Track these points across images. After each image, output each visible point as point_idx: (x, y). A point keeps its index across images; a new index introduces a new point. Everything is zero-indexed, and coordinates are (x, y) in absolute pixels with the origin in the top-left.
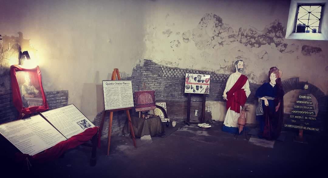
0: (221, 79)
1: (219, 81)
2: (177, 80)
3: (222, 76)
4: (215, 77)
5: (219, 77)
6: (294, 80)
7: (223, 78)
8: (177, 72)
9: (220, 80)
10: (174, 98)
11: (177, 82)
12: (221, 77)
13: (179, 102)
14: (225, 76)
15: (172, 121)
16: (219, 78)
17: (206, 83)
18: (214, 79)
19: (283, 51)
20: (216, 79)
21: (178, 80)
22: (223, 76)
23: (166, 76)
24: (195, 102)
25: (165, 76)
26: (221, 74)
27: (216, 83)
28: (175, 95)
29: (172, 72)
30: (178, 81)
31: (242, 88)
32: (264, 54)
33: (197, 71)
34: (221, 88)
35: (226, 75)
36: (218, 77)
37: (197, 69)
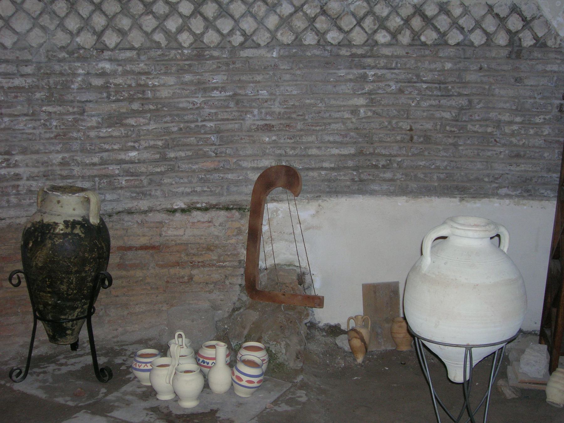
1: (344, 52)
2: (20, 62)
3: (362, 13)
4: (314, 19)
5: (339, 17)
9: (349, 44)
10: (13, 200)
11: (18, 82)
12: (359, 22)
13: (204, 83)
15: (464, 36)
16: (340, 29)
17: (189, 125)
18: (310, 39)
20: (321, 34)
21: (27, 63)
24: (185, 217)
27: (327, 64)
28: (18, 177)
30: (29, 70)
31: (99, 369)
32: (178, 215)
34: (362, 101)
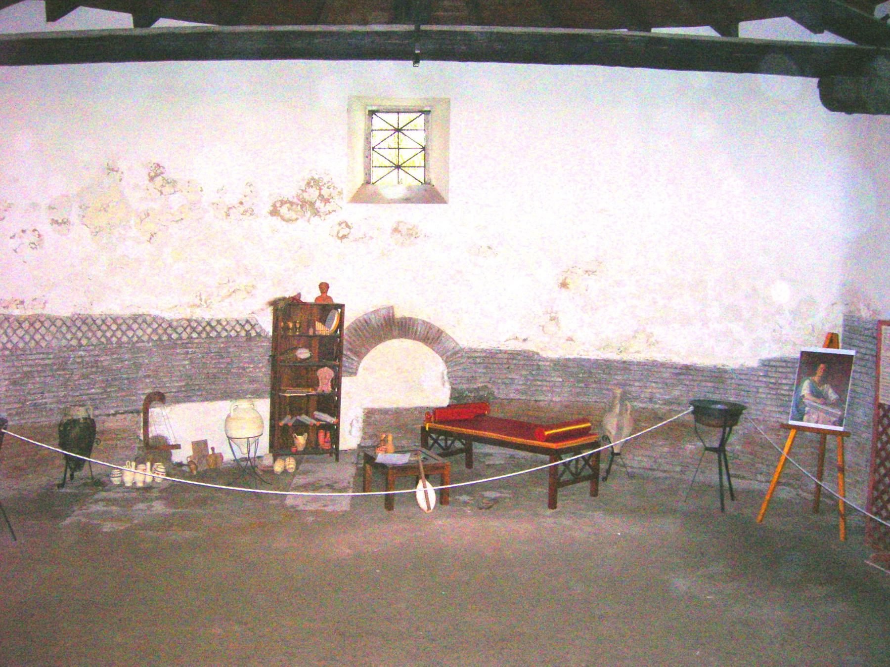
0: (184, 335)
1: (179, 342)
3: (185, 326)
6: (383, 312)
7: (188, 330)
8: (149, 331)
14: (194, 324)
16: (177, 333)
18: (165, 338)
19: (344, 237)
22: (189, 325)
23: (155, 338)
25: (150, 340)
26: (182, 319)
29: (145, 332)
33: (109, 319)
35: (196, 321)
36: (175, 330)
37: (108, 312)
